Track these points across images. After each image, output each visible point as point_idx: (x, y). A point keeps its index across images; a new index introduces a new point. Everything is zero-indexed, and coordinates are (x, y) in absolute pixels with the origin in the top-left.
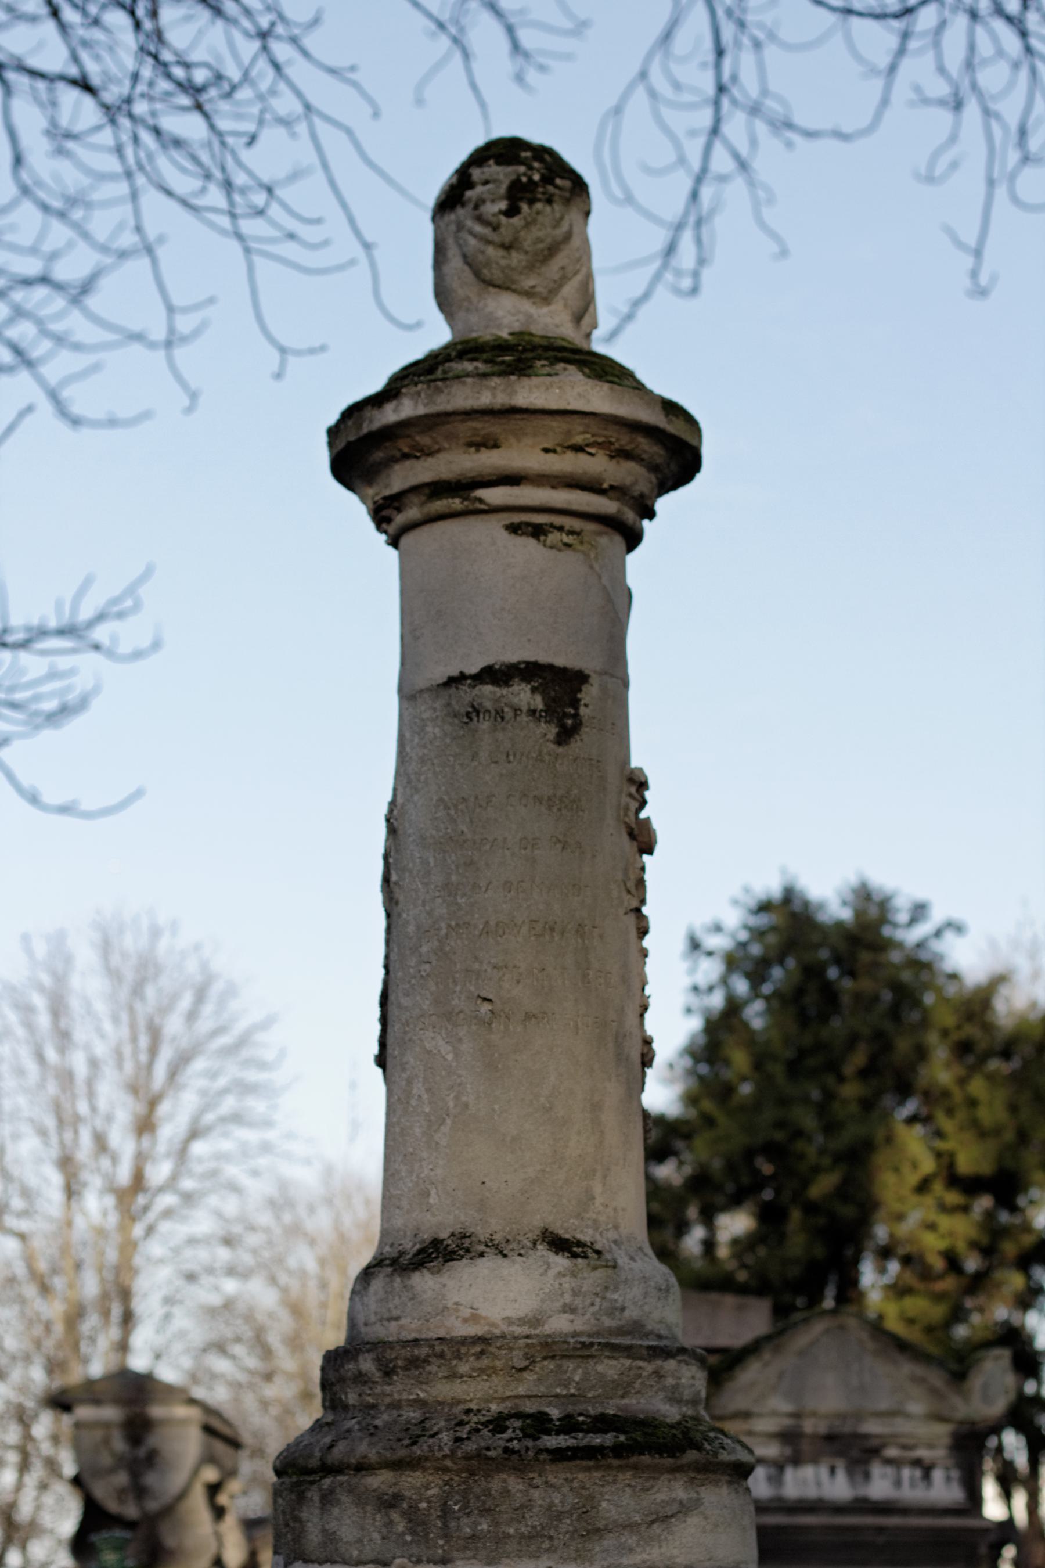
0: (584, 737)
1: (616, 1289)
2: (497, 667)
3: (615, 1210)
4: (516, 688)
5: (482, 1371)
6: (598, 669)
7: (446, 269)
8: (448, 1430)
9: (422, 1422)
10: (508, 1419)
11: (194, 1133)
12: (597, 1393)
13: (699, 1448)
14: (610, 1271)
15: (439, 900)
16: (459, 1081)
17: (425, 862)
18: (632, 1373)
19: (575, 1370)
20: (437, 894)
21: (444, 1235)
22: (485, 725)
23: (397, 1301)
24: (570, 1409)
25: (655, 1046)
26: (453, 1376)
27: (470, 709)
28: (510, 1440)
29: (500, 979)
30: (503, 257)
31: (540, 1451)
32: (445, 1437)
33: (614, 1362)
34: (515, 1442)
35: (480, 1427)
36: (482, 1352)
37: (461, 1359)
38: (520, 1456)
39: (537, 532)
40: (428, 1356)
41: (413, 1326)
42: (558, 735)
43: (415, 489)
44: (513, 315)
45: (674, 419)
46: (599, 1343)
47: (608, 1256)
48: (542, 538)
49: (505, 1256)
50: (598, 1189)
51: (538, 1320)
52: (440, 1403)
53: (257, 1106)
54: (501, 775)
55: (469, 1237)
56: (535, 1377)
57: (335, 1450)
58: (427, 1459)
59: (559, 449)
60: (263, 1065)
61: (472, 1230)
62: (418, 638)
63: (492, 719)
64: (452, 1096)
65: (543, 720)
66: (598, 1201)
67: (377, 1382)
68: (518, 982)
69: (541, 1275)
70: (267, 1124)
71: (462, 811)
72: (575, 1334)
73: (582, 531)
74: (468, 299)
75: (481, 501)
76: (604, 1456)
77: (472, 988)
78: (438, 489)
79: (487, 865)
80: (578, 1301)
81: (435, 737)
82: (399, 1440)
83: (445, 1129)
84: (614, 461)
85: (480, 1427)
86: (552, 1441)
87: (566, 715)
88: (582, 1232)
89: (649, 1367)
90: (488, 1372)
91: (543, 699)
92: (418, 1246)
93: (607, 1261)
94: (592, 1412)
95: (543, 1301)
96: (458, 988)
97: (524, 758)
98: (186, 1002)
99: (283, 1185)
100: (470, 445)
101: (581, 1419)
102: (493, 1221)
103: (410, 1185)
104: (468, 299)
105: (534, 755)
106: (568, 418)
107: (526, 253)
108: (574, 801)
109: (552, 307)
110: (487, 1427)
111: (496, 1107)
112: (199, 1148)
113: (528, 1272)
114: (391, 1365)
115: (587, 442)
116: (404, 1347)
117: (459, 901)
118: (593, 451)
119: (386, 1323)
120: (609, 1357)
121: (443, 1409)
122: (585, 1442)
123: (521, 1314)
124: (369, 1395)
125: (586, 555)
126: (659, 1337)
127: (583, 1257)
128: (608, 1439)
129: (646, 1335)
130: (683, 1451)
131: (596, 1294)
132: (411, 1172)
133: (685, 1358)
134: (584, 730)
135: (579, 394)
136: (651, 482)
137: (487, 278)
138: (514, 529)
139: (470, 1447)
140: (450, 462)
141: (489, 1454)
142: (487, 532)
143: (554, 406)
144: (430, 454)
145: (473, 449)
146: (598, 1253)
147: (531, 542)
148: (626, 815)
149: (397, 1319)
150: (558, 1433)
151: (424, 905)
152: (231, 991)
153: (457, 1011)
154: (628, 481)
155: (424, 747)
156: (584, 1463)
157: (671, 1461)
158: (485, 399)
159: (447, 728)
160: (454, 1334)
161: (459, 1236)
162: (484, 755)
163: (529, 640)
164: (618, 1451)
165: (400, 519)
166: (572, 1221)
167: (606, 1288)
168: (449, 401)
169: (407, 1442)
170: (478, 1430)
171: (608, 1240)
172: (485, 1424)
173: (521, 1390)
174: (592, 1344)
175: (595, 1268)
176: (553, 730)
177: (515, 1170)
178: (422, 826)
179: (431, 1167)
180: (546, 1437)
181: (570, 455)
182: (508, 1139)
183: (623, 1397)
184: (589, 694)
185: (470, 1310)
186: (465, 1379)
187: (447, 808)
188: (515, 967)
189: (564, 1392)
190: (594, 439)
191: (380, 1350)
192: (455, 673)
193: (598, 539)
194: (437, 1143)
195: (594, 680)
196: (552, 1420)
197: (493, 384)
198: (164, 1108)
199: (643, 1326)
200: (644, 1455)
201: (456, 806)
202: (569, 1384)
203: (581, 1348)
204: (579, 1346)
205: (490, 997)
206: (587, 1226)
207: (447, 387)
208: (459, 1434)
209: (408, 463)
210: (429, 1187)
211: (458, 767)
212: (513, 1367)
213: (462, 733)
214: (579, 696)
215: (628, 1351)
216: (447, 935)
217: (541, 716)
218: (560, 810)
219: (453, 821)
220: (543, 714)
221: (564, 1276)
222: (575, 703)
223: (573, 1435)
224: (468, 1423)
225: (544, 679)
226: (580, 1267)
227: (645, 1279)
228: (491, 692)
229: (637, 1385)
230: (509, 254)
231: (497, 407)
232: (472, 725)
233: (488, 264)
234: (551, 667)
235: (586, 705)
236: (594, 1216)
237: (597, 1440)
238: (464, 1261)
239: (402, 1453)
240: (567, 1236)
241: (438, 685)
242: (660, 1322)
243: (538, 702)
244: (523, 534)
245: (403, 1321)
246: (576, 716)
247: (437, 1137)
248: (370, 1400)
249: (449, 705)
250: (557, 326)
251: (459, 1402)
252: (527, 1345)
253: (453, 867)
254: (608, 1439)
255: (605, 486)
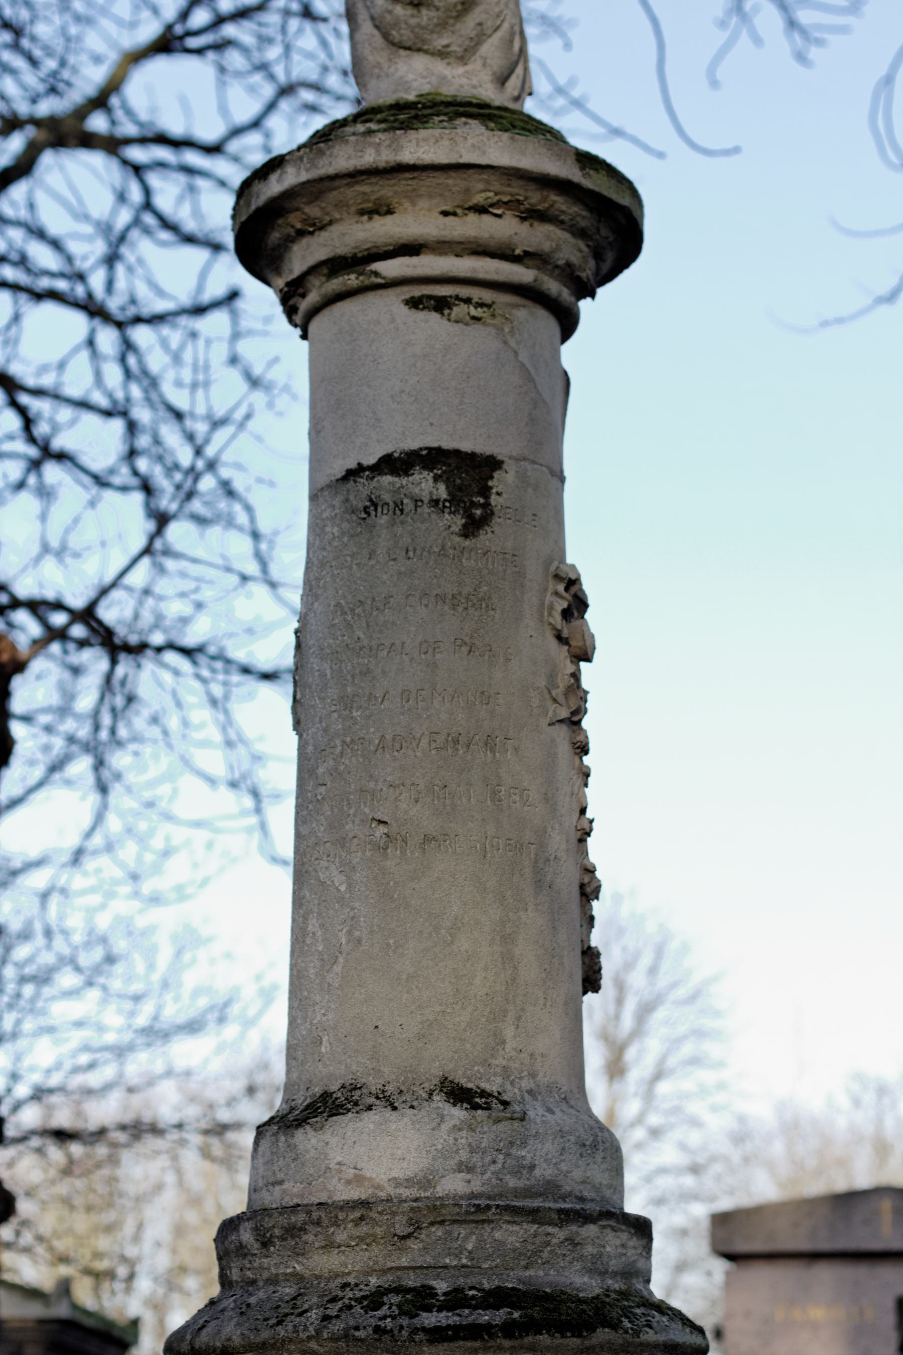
0: (496, 528)
1: (524, 1144)
2: (396, 455)
3: (532, 1055)
4: (416, 477)
5: (361, 1239)
6: (514, 454)
7: (359, 36)
8: (318, 1307)
9: (295, 1298)
10: (386, 1294)
11: (658, 1075)
12: (494, 1264)
13: (615, 1326)
14: (516, 1124)
15: (335, 715)
16: (351, 914)
17: (323, 675)
18: (538, 1240)
19: (467, 1238)
20: (333, 708)
21: (334, 1087)
22: (383, 520)
23: (281, 1163)
24: (461, 1281)
25: (598, 874)
26: (330, 1246)
27: (368, 504)
28: (384, 1317)
29: (396, 799)
30: (412, 16)
31: (415, 1331)
32: (314, 1315)
33: (516, 1228)
34: (389, 1320)
35: (353, 1303)
36: (362, 1218)
37: (339, 1226)
38: (393, 1336)
39: (441, 305)
40: (305, 1223)
41: (295, 1190)
42: (465, 526)
43: (313, 270)
44: (425, 78)
45: (592, 172)
46: (498, 1206)
47: (517, 1108)
48: (446, 312)
49: (395, 1109)
50: (509, 1033)
51: (429, 1181)
52: (318, 1277)
53: (713, 1049)
54: (400, 573)
55: (360, 1088)
56: (421, 1245)
57: (204, 1332)
58: (291, 1340)
59: (459, 211)
60: (717, 1014)
61: (364, 1080)
62: (320, 432)
63: (391, 512)
64: (345, 930)
65: (447, 510)
66: (508, 1047)
67: (255, 1254)
68: (416, 802)
69: (433, 1129)
70: (720, 1065)
71: (358, 615)
72: (473, 1196)
73: (493, 303)
74: (379, 65)
75: (376, 274)
76: (492, 1336)
77: (367, 810)
78: (336, 265)
79: (384, 672)
80: (476, 1159)
81: (334, 538)
82: (266, 1319)
83: (337, 969)
84: (527, 224)
85: (353, 1303)
86: (430, 1319)
87: (473, 505)
88: (488, 1080)
89: (560, 1234)
90: (368, 1241)
91: (447, 487)
92: (308, 1101)
93: (514, 1112)
94: (487, 1286)
95: (434, 1159)
96: (352, 812)
97: (425, 554)
98: (646, 961)
99: (742, 1119)
100: (362, 212)
101: (471, 1293)
102: (386, 1070)
103: (304, 1033)
104: (379, 65)
105: (437, 550)
106: (462, 174)
107: (438, 9)
108: (483, 599)
109: (468, 68)
110: (361, 1303)
111: (391, 941)
112: (663, 1088)
113: (418, 1126)
114: (268, 1235)
115: (490, 201)
116: (280, 1214)
117: (355, 714)
118: (499, 212)
119: (271, 1187)
120: (509, 1222)
121: (319, 1283)
122: (470, 1319)
123: (410, 1174)
124: (249, 1269)
125: (500, 329)
126: (582, 1199)
127: (483, 1109)
128: (499, 1316)
129: (564, 1198)
130: (592, 1329)
131: (499, 1151)
132: (305, 1019)
133: (612, 1223)
134: (496, 520)
135: (473, 146)
136: (580, 251)
137: (396, 40)
138: (414, 303)
139: (337, 1326)
140: (343, 234)
141: (357, 1334)
142: (388, 307)
143: (444, 159)
144: (322, 228)
145: (365, 218)
146: (505, 1104)
147: (434, 316)
148: (550, 615)
149: (281, 1183)
150: (440, 1310)
151: (321, 722)
152: (685, 948)
153: (351, 835)
154: (547, 247)
155: (324, 549)
156: (469, 1344)
157: (575, 1342)
158: (369, 158)
159: (346, 526)
160: (336, 1198)
161: (349, 1088)
162: (381, 552)
163: (431, 424)
164: (509, 1329)
165: (304, 305)
166: (476, 1068)
167: (511, 1143)
168: (331, 163)
169: (273, 1321)
170: (350, 1307)
171: (520, 1089)
172: (359, 1301)
173: (404, 1262)
174: (488, 1207)
175: (498, 1121)
176: (459, 522)
177: (412, 1012)
178: (320, 635)
179: (323, 1011)
180: (425, 1314)
181: (472, 217)
182: (404, 977)
183: (526, 1268)
184: (503, 482)
185: (353, 1171)
186: (343, 1248)
187: (344, 613)
188: (413, 784)
189: (455, 1263)
190: (498, 198)
191: (259, 1218)
192: (353, 465)
193: (514, 311)
194: (329, 985)
195: (509, 466)
196: (437, 1294)
197: (377, 140)
198: (631, 1054)
199: (559, 1187)
200: (541, 1334)
201: (352, 610)
202: (461, 1253)
203: (476, 1212)
204: (473, 1210)
205: (385, 819)
206: (495, 1074)
207: (329, 149)
208: (329, 1312)
209: (305, 241)
210: (321, 1034)
211: (355, 567)
212: (395, 1235)
213: (359, 530)
214: (490, 483)
215: (534, 1215)
216: (342, 753)
217: (444, 507)
218: (466, 609)
219: (349, 626)
220: (447, 504)
221: (460, 1130)
222: (485, 491)
223: (458, 1311)
224: (342, 1298)
225: (450, 465)
226: (479, 1119)
227: (562, 1133)
228: (389, 483)
229: (545, 1255)
230: (419, 11)
231: (382, 165)
232: (369, 521)
233: (396, 24)
234: (457, 453)
235: (498, 494)
236: (504, 1063)
237: (485, 1317)
238: (350, 1114)
239: (265, 1334)
240: (470, 1085)
241: (337, 480)
242: (584, 1182)
243: (442, 491)
244: (424, 308)
245: (286, 1185)
246: (486, 505)
247: (330, 977)
248: (249, 1274)
249: (347, 500)
250: (474, 87)
251: (337, 1275)
252: (412, 1209)
253: (349, 677)
254: (499, 1316)
255: (518, 252)
